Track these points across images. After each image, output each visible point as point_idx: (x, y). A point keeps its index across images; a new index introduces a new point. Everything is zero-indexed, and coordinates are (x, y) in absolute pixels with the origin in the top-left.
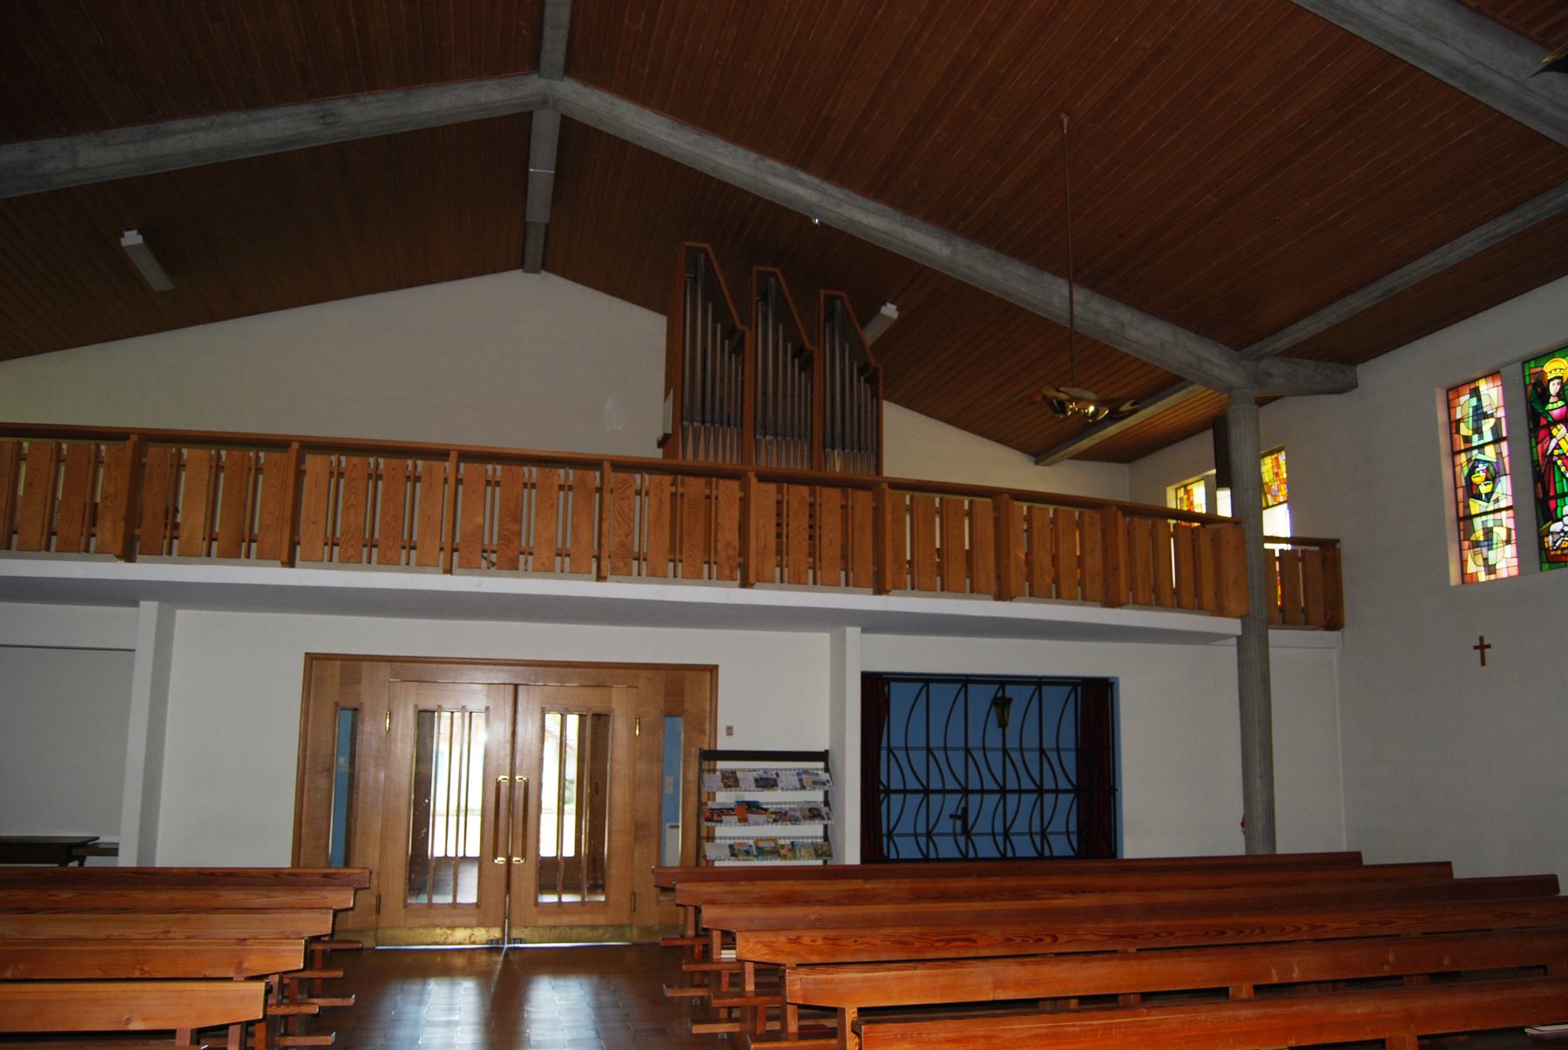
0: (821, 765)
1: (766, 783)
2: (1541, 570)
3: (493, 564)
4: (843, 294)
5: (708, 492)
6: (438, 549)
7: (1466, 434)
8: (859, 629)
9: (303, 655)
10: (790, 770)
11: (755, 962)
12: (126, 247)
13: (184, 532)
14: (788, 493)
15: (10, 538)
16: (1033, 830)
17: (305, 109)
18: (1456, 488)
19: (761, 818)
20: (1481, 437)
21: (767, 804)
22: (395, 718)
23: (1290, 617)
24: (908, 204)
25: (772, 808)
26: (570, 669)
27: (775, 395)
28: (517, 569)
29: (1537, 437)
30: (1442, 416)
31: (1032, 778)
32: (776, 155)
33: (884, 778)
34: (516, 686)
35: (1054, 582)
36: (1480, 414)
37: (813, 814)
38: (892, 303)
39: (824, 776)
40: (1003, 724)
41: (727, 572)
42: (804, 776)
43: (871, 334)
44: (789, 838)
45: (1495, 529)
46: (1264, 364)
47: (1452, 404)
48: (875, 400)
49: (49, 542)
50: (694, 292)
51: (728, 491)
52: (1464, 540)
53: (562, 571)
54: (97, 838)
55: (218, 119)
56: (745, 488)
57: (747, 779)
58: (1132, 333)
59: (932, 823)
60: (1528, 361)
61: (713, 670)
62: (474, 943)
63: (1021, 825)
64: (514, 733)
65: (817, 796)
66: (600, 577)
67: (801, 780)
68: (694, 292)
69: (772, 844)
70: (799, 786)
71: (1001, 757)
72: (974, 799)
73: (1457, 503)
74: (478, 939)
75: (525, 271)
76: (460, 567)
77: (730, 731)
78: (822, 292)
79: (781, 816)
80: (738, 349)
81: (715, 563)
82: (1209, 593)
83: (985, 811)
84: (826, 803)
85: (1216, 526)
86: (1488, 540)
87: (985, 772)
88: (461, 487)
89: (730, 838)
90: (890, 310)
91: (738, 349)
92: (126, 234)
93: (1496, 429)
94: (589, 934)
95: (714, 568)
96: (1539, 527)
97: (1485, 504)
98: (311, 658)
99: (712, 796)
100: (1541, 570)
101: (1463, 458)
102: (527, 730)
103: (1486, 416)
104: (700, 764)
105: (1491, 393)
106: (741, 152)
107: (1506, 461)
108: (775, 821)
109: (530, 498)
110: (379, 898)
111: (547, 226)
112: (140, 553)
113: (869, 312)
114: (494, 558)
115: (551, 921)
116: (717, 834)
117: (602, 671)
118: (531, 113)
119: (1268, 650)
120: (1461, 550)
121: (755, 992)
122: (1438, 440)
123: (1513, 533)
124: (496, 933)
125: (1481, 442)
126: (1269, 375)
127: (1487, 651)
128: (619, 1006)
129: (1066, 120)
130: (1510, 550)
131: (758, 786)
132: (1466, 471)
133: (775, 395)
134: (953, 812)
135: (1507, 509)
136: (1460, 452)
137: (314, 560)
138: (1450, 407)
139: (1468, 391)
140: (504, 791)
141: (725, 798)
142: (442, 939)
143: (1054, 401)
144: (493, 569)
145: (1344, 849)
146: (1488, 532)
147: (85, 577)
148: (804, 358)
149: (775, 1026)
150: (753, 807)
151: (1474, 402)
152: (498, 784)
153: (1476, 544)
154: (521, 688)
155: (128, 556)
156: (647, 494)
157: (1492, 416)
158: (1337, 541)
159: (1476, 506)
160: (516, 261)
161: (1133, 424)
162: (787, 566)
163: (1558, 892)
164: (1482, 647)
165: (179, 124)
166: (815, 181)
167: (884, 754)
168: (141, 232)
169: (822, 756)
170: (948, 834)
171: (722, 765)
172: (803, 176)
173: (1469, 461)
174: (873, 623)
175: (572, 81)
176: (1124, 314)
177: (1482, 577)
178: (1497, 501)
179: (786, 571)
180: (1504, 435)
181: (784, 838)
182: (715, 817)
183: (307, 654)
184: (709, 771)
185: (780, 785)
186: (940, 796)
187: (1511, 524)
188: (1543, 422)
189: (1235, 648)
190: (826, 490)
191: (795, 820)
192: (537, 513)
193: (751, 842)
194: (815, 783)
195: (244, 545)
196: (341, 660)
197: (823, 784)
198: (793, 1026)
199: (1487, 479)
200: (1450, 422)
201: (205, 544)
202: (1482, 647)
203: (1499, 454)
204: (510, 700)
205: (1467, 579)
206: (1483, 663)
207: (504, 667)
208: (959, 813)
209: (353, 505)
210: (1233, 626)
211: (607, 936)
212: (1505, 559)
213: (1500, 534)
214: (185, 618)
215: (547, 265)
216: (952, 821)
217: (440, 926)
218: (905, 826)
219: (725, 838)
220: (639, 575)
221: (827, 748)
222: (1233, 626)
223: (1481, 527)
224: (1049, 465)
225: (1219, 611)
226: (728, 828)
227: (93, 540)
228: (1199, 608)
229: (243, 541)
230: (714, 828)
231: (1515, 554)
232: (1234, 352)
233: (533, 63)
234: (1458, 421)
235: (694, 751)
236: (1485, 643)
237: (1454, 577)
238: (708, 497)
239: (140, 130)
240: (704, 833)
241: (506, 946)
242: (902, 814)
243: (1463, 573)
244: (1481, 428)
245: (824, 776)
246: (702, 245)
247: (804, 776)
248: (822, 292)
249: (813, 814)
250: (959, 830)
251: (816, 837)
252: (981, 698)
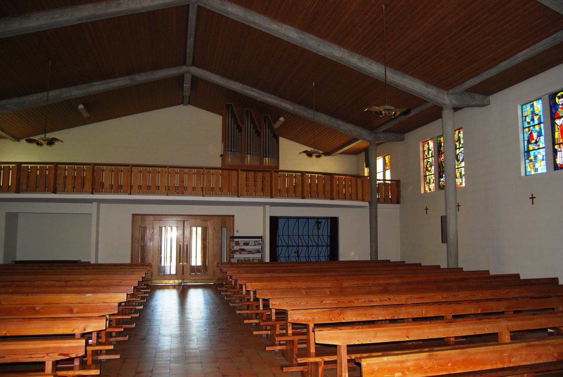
0: (261, 240)
1: (246, 244)
2: (439, 190)
3: (178, 193)
4: (269, 115)
5: (229, 174)
6: (165, 189)
7: (528, 121)
8: (269, 206)
9: (132, 214)
10: (253, 241)
11: (276, 309)
12: (80, 109)
13: (105, 187)
14: (249, 174)
15: (64, 189)
16: (326, 256)
17: (127, 78)
18: (424, 168)
19: (245, 253)
20: (429, 156)
21: (247, 249)
22: (154, 229)
23: (386, 201)
24: (282, 96)
25: (248, 250)
26: (197, 217)
27: (250, 143)
28: (183, 194)
29: (439, 157)
30: (421, 149)
31: (316, 243)
32: (247, 85)
33: (277, 244)
34: (184, 221)
35: (317, 194)
36: (429, 150)
37: (258, 251)
38: (282, 117)
39: (261, 242)
40: (319, 229)
41: (234, 194)
42: (256, 242)
43: (276, 126)
44: (252, 258)
45: (538, 156)
46: (378, 134)
47: (424, 146)
48: (277, 144)
49: (74, 190)
50: (229, 114)
51: (234, 173)
52: (527, 159)
53: (194, 194)
54: (81, 260)
55: (105, 81)
56: (238, 173)
57: (241, 243)
58: (342, 128)
59: (289, 254)
60: (438, 137)
61: (233, 216)
62: (175, 283)
63: (313, 254)
64: (184, 233)
65: (259, 247)
66: (203, 196)
67: (255, 243)
68: (229, 114)
69: (248, 259)
70: (254, 245)
71: (317, 237)
72: (300, 248)
73: (424, 172)
74: (176, 283)
75: (184, 105)
76: (170, 194)
77: (237, 231)
78: (263, 115)
79: (250, 252)
80: (241, 130)
81: (231, 191)
82: (360, 195)
83: (303, 252)
84: (262, 249)
85: (363, 178)
86: (535, 159)
87: (323, 241)
88: (169, 174)
89: (238, 258)
90: (282, 119)
91: (241, 130)
92: (80, 105)
93: (539, 119)
94: (203, 281)
95: (231, 192)
96: (439, 179)
97: (429, 173)
98: (133, 215)
99: (233, 247)
100: (439, 190)
101: (425, 160)
102: (187, 232)
103: (430, 150)
104: (230, 240)
105: (431, 144)
106: (238, 84)
107: (433, 162)
108: (248, 253)
109: (186, 177)
110: (152, 273)
111: (189, 97)
112: (95, 192)
113: (276, 120)
114: (178, 191)
115: (194, 278)
116: (234, 257)
117: (205, 217)
118: (184, 75)
119: (377, 210)
120: (525, 163)
121: (275, 320)
122: (518, 124)
123: (544, 157)
124: (180, 281)
125: (534, 124)
126: (380, 137)
127: (534, 199)
128: (230, 331)
129: (384, 8)
130: (544, 163)
131: (244, 245)
132: (426, 164)
133: (250, 143)
134: (295, 251)
135: (433, 174)
136: (425, 159)
137: (135, 193)
138: (423, 147)
139: (529, 106)
140: (182, 247)
141: (236, 248)
142: (167, 283)
143: (374, 112)
144: (178, 194)
145: (399, 260)
146: (535, 157)
147: (366, 320)
148: (258, 133)
149: (284, 332)
150: (243, 250)
151: (532, 109)
152: (180, 245)
153: (531, 161)
154: (185, 221)
155: (92, 193)
156: (214, 175)
157: (537, 115)
158: (400, 180)
159: (428, 173)
160: (182, 103)
161: (351, 147)
162: (249, 192)
163: (558, 283)
164: (532, 198)
165: (96, 83)
166: (257, 90)
167: (277, 236)
168: (83, 105)
169: (261, 237)
170: (294, 257)
171: (235, 240)
172: (254, 89)
173: (427, 161)
174: (272, 204)
175: (194, 67)
176: (340, 122)
177: (533, 173)
178: (431, 172)
179: (248, 193)
180: (433, 155)
181: (251, 258)
182: (234, 253)
183: (132, 214)
184: (232, 241)
185: (250, 245)
186: (292, 247)
187: (434, 178)
188: (440, 153)
189: (369, 209)
190: (258, 173)
191: (253, 253)
192: (188, 180)
193: (243, 259)
194: (258, 244)
195: (119, 190)
196: (141, 215)
197: (261, 244)
198: (290, 332)
199: (430, 166)
200: (423, 151)
201: (110, 189)
202: (532, 198)
203: (540, 128)
204: (182, 224)
205: (426, 192)
206: (533, 204)
207: (181, 217)
208: (297, 251)
209: (144, 180)
210: (366, 204)
211: (208, 282)
212: (541, 167)
213: (540, 157)
214: (102, 206)
215: (190, 103)
216: (295, 253)
217: (167, 280)
218: (282, 255)
219: (236, 258)
220: (212, 195)
221: (262, 235)
222: (366, 204)
223: (533, 155)
224: (333, 156)
225: (363, 200)
226: (237, 255)
227: (84, 189)
228: (357, 199)
229: (119, 188)
230: (234, 255)
231: (545, 165)
232: (370, 131)
233: (184, 63)
234: (425, 151)
235: (229, 236)
236: (534, 196)
237: (523, 174)
238: (229, 175)
239: (87, 85)
240: (231, 257)
241: (183, 284)
242: (282, 252)
243: (425, 190)
244: (534, 119)
245: (261, 242)
246: (231, 103)
247: (256, 242)
248: (263, 115)
249: (258, 251)
250: (296, 256)
251: (259, 257)
252: (312, 222)
